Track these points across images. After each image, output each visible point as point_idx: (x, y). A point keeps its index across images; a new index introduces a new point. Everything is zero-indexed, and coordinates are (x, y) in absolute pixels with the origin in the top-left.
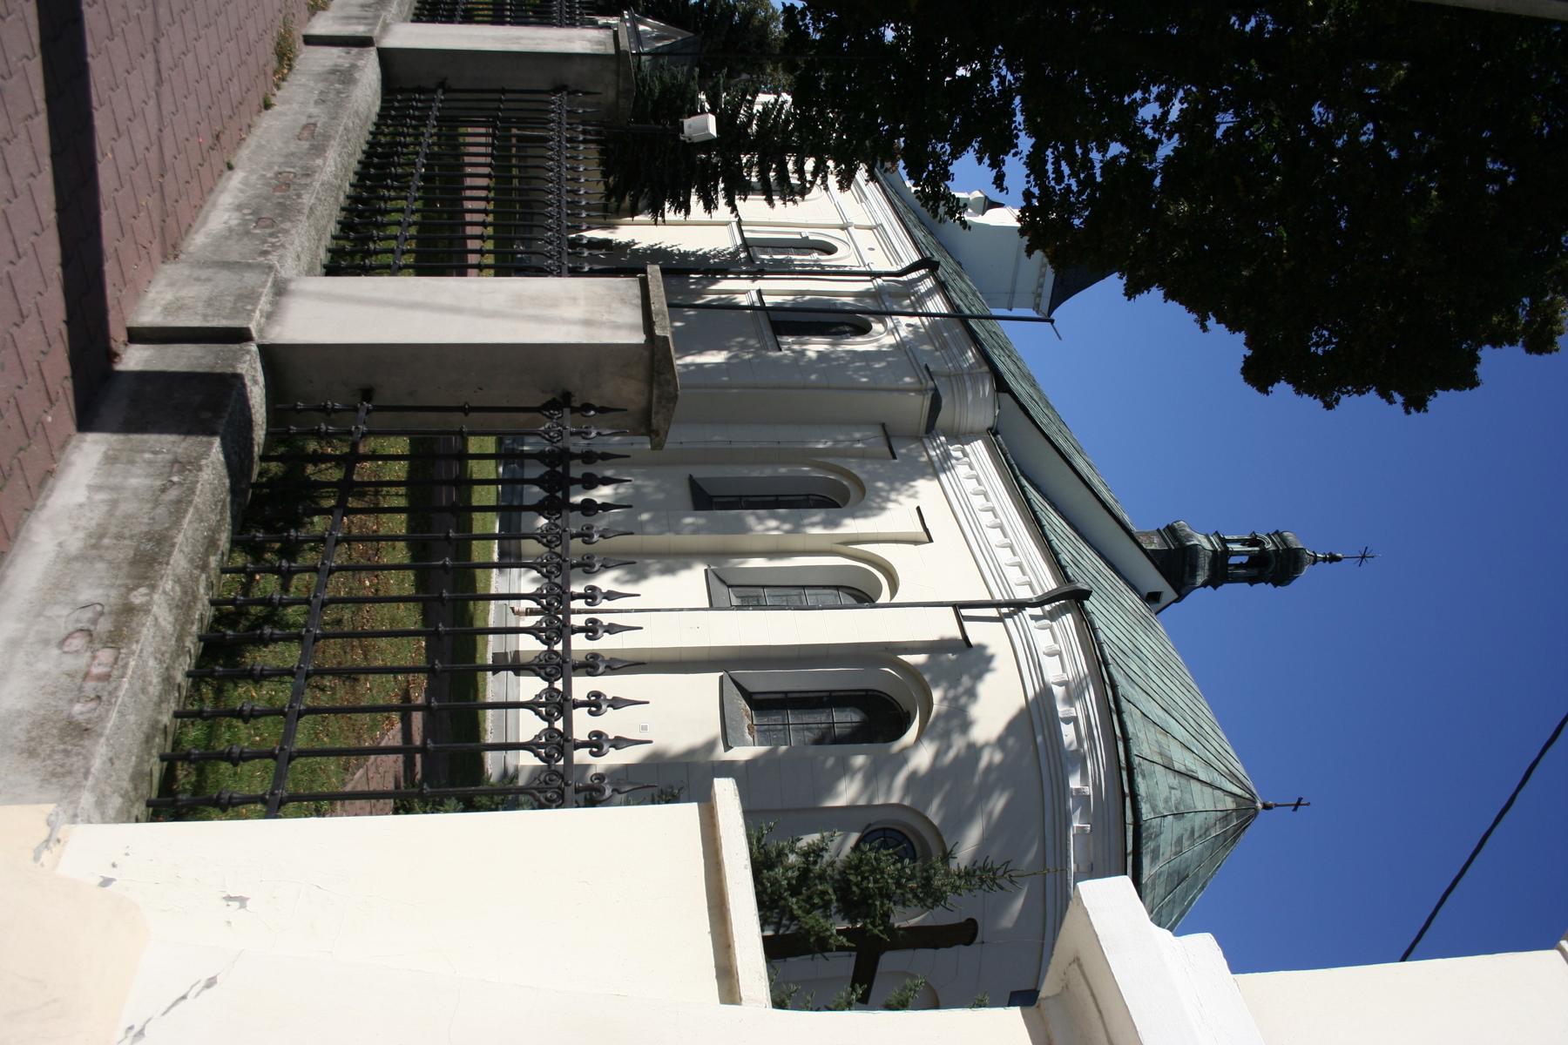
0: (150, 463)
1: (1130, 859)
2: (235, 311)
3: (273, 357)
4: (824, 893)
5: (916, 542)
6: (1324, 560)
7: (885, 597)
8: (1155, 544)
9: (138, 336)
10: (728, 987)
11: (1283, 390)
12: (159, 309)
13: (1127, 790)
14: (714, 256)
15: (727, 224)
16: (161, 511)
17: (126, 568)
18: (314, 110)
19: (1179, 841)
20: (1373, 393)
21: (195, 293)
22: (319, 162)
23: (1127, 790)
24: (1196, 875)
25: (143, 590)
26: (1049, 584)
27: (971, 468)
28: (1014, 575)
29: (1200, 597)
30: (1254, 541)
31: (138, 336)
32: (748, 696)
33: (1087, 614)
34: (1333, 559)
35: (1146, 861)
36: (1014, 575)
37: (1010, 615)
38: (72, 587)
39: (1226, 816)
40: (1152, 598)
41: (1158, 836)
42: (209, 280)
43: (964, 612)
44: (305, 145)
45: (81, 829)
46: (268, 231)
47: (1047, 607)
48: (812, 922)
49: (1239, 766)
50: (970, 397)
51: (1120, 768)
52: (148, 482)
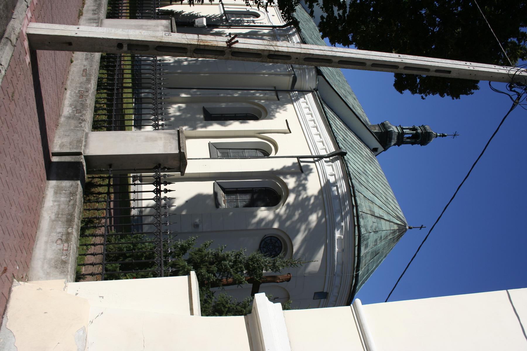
0: (65, 194)
1: (356, 248)
2: (78, 147)
3: (87, 158)
4: (241, 267)
5: (285, 133)
6: (440, 136)
7: (273, 154)
8: (377, 130)
9: (55, 154)
10: (192, 313)
11: (407, 92)
12: (58, 146)
13: (356, 224)
14: (213, 18)
15: (218, 4)
16: (70, 207)
17: (65, 223)
18: (85, 63)
19: (376, 240)
20: (438, 94)
21: (66, 140)
22: (89, 86)
23: (356, 224)
24: (382, 252)
25: (70, 228)
26: (333, 149)
27: (307, 104)
28: (320, 145)
29: (393, 149)
30: (414, 129)
31: (55, 154)
32: (223, 189)
33: (345, 161)
34: (443, 136)
35: (362, 248)
36: (320, 145)
37: (317, 161)
38: (55, 228)
39: (394, 232)
40: (374, 150)
41: (367, 239)
42: (68, 136)
43: (301, 160)
44: (85, 78)
45: (69, 283)
46: (80, 114)
47: (331, 158)
48: (237, 277)
49: (401, 213)
50: (307, 77)
51: (354, 216)
52: (65, 199)
